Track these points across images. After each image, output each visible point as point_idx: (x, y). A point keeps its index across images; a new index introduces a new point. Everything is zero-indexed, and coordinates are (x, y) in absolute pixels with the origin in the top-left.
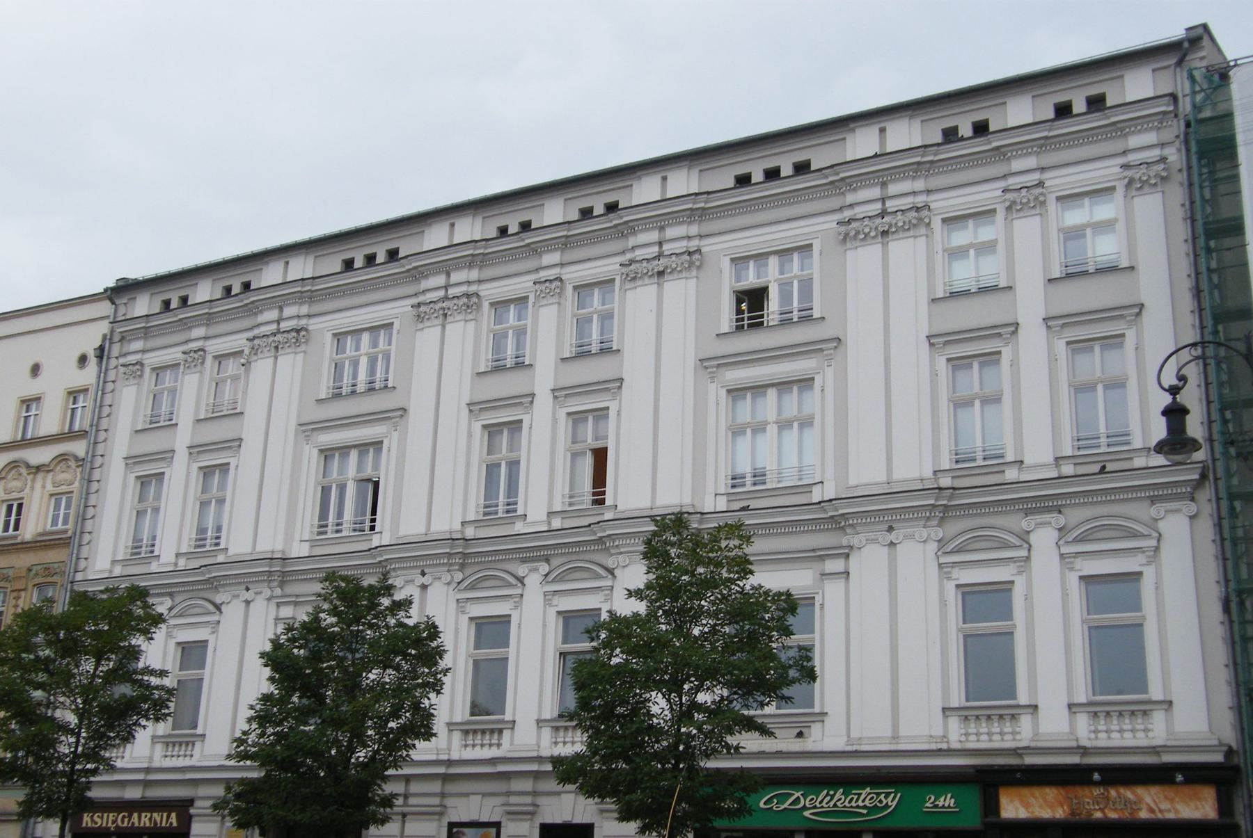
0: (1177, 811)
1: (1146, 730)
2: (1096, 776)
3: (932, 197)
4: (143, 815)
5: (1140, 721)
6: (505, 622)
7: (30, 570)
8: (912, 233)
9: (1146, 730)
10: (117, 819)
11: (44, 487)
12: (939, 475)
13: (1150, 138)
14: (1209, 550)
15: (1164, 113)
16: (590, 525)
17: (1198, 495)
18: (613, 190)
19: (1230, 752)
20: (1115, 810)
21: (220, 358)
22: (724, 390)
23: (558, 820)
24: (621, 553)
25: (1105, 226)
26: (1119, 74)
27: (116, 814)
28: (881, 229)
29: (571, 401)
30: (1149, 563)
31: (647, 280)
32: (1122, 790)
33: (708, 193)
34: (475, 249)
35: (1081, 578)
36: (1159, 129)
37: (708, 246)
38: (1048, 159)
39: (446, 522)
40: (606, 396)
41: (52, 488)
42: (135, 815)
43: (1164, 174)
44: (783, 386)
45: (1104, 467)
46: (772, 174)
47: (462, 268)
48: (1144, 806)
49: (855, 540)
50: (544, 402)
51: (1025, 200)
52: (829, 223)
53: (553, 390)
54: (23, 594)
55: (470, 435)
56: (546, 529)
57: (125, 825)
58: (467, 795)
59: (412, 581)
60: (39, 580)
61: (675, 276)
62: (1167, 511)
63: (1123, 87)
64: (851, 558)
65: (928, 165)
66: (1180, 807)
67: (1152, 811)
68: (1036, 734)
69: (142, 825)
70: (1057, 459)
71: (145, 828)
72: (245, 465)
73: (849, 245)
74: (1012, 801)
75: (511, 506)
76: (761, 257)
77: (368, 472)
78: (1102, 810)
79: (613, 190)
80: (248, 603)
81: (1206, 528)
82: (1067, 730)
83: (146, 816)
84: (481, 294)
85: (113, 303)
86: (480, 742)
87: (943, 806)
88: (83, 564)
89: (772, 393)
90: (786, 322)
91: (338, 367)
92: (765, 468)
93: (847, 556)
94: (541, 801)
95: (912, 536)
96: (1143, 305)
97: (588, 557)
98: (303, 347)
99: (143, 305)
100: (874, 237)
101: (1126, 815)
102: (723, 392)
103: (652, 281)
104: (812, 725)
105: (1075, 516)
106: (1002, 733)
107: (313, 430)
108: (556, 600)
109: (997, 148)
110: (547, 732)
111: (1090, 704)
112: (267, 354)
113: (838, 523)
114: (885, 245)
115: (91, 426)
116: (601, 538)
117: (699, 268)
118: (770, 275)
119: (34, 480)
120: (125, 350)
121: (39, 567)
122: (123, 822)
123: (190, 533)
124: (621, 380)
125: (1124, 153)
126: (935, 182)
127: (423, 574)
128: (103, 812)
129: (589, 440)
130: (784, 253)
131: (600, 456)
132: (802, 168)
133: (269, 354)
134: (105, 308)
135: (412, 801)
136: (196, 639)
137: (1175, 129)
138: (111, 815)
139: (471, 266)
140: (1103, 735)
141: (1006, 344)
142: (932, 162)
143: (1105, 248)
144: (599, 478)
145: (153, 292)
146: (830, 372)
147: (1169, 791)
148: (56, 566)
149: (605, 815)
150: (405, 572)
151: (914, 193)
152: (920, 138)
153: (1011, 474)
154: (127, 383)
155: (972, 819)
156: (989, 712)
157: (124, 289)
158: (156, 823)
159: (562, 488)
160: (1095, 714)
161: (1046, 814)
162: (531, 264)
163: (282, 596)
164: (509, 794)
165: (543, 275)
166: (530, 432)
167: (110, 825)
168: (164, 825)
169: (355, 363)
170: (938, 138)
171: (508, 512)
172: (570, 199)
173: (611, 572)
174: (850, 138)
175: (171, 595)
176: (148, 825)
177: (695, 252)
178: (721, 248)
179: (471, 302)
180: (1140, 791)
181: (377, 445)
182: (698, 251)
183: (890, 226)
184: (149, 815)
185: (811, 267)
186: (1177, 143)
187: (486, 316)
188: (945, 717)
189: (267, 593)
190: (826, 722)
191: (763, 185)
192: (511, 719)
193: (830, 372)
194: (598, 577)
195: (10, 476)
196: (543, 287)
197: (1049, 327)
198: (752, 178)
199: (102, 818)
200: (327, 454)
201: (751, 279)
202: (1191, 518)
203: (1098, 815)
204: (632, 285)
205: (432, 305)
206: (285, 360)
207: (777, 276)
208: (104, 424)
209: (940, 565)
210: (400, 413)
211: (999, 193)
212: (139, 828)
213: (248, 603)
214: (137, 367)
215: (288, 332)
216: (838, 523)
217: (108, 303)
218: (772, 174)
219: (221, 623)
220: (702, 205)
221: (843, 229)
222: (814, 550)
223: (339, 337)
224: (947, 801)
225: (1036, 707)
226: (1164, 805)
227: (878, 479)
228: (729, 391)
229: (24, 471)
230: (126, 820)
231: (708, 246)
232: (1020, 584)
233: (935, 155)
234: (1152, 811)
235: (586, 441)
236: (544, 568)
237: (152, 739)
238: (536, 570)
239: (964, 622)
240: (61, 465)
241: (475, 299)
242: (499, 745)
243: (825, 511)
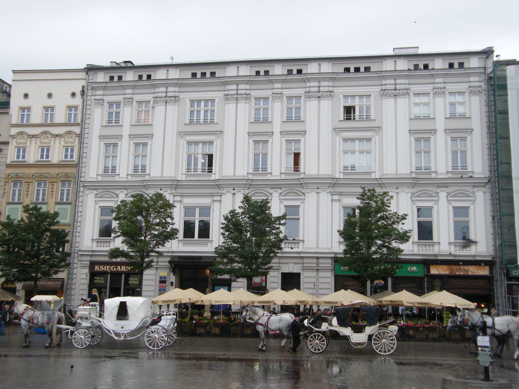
0: (479, 273)
1: (470, 250)
3: (180, 94)
4: (122, 267)
7: (9, 175)
8: (404, 97)
9: (470, 250)
10: (110, 268)
11: (36, 143)
13: (476, 79)
14: (489, 202)
15: (482, 72)
22: (342, 139)
23: (288, 271)
25: (461, 103)
26: (381, 61)
29: (135, 139)
31: (314, 99)
32: (464, 267)
33: (337, 73)
34: (136, 83)
35: (453, 207)
37: (336, 90)
38: (447, 80)
40: (117, 140)
41: (64, 144)
42: (119, 267)
43: (481, 91)
44: (361, 140)
45: (462, 176)
46: (357, 70)
47: (244, 84)
48: (470, 271)
49: (224, 192)
50: (126, 139)
51: (440, 92)
52: (378, 89)
53: (129, 135)
55: (249, 143)
57: (115, 270)
58: (288, 263)
60: (63, 179)
61: (324, 99)
62: (322, 191)
63: (470, 60)
66: (480, 271)
67: (472, 272)
69: (122, 270)
70: (447, 172)
72: (155, 144)
73: (383, 97)
75: (265, 169)
76: (353, 97)
77: (207, 152)
78: (459, 272)
80: (234, 194)
81: (488, 196)
82: (448, 250)
84: (104, 99)
85: (87, 74)
88: (83, 175)
89: (357, 141)
90: (361, 119)
91: (192, 112)
92: (355, 165)
94: (281, 265)
95: (404, 191)
96: (445, 130)
97: (295, 188)
98: (177, 104)
99: (101, 77)
100: (392, 96)
102: (341, 139)
103: (316, 99)
105: (451, 189)
106: (429, 250)
107: (340, 131)
108: (284, 202)
109: (432, 74)
110: (95, 243)
111: (454, 243)
112: (162, 104)
114: (319, 101)
116: (301, 183)
118: (356, 103)
120: (94, 93)
121: (37, 174)
122: (113, 269)
123: (131, 167)
124: (306, 132)
125: (124, 94)
126: (136, 91)
127: (234, 189)
128: (104, 266)
129: (293, 150)
130: (361, 96)
131: (297, 156)
133: (163, 104)
134: (83, 75)
135: (159, 264)
137: (483, 77)
138: (108, 267)
139: (247, 83)
140: (421, 251)
141: (433, 136)
143: (460, 110)
144: (296, 162)
147: (477, 267)
148: (70, 174)
150: (227, 188)
151: (405, 84)
152: (103, 79)
153: (433, 175)
154: (97, 107)
155: (421, 274)
157: (91, 69)
159: (284, 165)
160: (456, 245)
161: (443, 273)
163: (176, 193)
165: (126, 96)
166: (121, 148)
167: (108, 270)
169: (199, 112)
170: (286, 73)
173: (304, 194)
174: (309, 65)
175: (126, 189)
177: (177, 97)
178: (340, 91)
179: (247, 97)
180: (469, 267)
183: (322, 95)
184: (125, 267)
186: (485, 82)
187: (253, 102)
188: (413, 244)
189: (170, 191)
192: (302, 239)
193: (377, 137)
194: (300, 195)
196: (275, 95)
197: (445, 132)
201: (349, 103)
203: (458, 273)
204: (309, 99)
205: (232, 96)
206: (170, 107)
207: (358, 103)
208: (87, 121)
213: (234, 194)
214: (280, 95)
215: (171, 97)
216: (218, 186)
217: (85, 73)
220: (335, 76)
221: (382, 92)
223: (192, 102)
224: (414, 268)
225: (439, 243)
226: (476, 271)
227: (158, 176)
228: (187, 142)
229: (50, 136)
230: (115, 268)
231: (181, 95)
233: (413, 73)
234: (472, 272)
235: (292, 150)
236: (126, 192)
238: (277, 191)
242: (109, 246)
243: (216, 183)
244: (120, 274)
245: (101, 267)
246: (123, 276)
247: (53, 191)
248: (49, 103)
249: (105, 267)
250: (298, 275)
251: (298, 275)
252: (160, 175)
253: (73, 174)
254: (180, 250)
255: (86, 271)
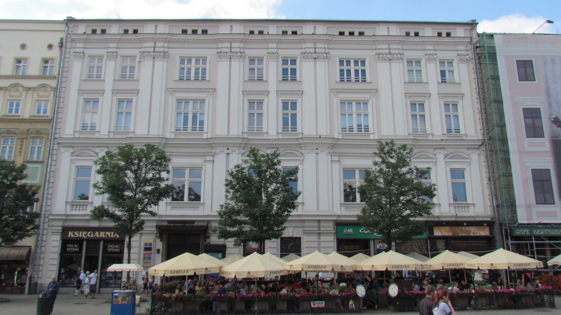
0: (480, 233)
1: (468, 212)
2: (465, 224)
4: (101, 233)
5: (466, 209)
6: (90, 168)
9: (468, 212)
10: (87, 234)
11: (33, 96)
12: (409, 135)
16: (126, 138)
17: (480, 148)
18: (413, 28)
19: (492, 218)
20: (465, 233)
21: (123, 57)
24: (307, 149)
27: (86, 232)
28: (314, 57)
30: (301, 164)
31: (310, 60)
32: (466, 228)
36: (465, 46)
38: (437, 47)
39: (235, 132)
42: (97, 233)
46: (351, 34)
48: (471, 232)
50: (273, 95)
54: (25, 140)
55: (243, 102)
56: (108, 137)
57: (92, 236)
59: (223, 151)
61: (321, 60)
62: (321, 152)
64: (215, 156)
65: (403, 42)
66: (480, 232)
67: (474, 233)
68: (440, 212)
69: (101, 236)
71: (102, 238)
74: (437, 231)
78: (461, 233)
79: (413, 28)
80: (228, 154)
81: (483, 158)
83: (102, 233)
85: (67, 25)
86: (78, 209)
87: (349, 232)
88: (58, 131)
93: (214, 156)
97: (89, 149)
101: (467, 234)
104: (200, 207)
107: (173, 91)
113: (211, 146)
115: (59, 74)
117: (168, 58)
119: (26, 94)
122: (90, 235)
127: (228, 149)
128: (79, 231)
132: (205, 32)
136: (84, 165)
138: (84, 233)
139: (241, 42)
142: (404, 41)
145: (433, 28)
146: (211, 99)
149: (305, 234)
156: (465, 205)
157: (70, 21)
158: (108, 235)
161: (446, 234)
162: (105, 45)
163: (333, 153)
164: (304, 227)
168: (112, 236)
171: (91, 129)
172: (279, 26)
176: (104, 236)
180: (470, 228)
181: (366, 103)
182: (167, 52)
184: (104, 233)
185: (102, 62)
190: (204, 207)
191: (337, 37)
195: (12, 90)
198: (288, 32)
199: (79, 233)
200: (179, 101)
202: (478, 155)
203: (460, 234)
209: (445, 162)
210: (213, 90)
211: (216, 53)
212: (99, 238)
214: (82, 54)
216: (211, 146)
217: (64, 25)
218: (195, 32)
219: (437, 162)
220: (331, 39)
222: (203, 153)
226: (477, 232)
229: (21, 89)
230: (92, 235)
232: (468, 169)
234: (474, 233)
236: (71, 150)
237: (66, 203)
238: (103, 150)
239: (189, 178)
240: (42, 88)
241: (243, 54)
243: (299, 142)
244: (97, 241)
245: (75, 233)
246: (102, 243)
247: (21, 149)
248: (22, 54)
249: (81, 232)
250: (299, 239)
251: (299, 239)
252: (393, 134)
253: (46, 130)
254: (168, 214)
255: (58, 238)
